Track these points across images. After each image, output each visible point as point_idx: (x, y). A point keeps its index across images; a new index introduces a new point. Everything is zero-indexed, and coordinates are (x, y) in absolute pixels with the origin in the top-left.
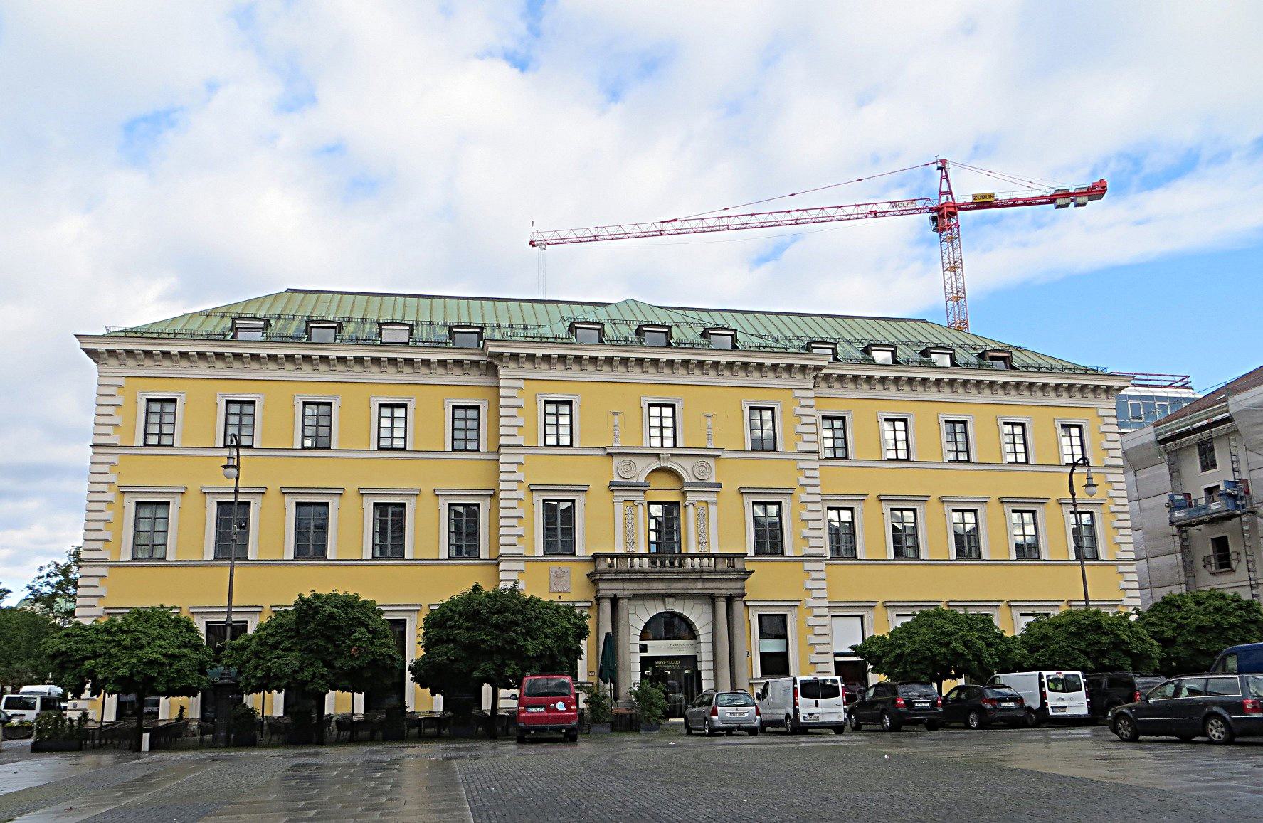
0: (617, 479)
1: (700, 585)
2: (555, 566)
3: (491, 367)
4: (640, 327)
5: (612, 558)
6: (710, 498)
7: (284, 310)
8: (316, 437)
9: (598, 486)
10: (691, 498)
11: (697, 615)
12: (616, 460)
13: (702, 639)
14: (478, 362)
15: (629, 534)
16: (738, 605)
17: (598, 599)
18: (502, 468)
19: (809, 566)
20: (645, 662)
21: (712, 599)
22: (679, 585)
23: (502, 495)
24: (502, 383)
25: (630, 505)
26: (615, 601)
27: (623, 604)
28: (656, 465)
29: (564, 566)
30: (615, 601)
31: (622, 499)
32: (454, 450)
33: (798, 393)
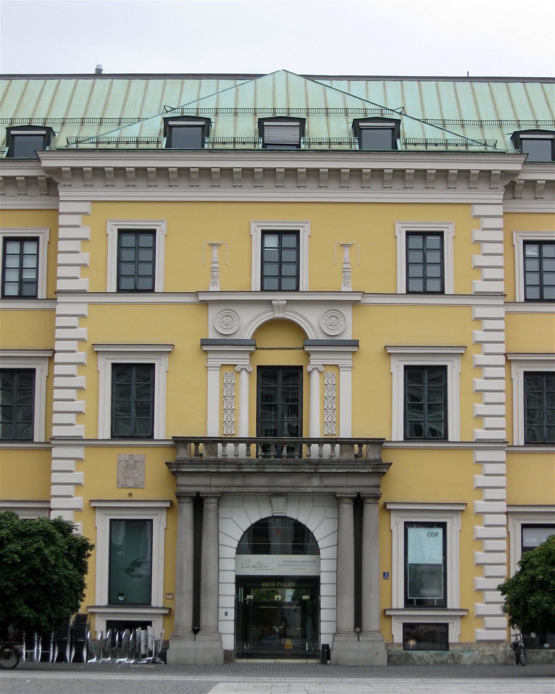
0: (212, 336)
1: (316, 481)
2: (125, 453)
3: (50, 183)
4: (356, 122)
5: (360, 445)
6: (344, 361)
7: (16, 111)
8: (21, 282)
9: (187, 346)
10: (316, 361)
11: (319, 523)
12: (213, 312)
13: (324, 553)
14: (35, 178)
15: (228, 411)
16: (371, 512)
17: (179, 496)
18: (59, 322)
19: (481, 456)
20: (244, 583)
21: (336, 500)
22: (287, 481)
23: (58, 357)
24: (62, 207)
25: (229, 371)
26: (198, 502)
27: (210, 506)
28: (268, 316)
29: (137, 453)
30: (198, 502)
31: (219, 363)
32: (409, 292)
33: (479, 210)
